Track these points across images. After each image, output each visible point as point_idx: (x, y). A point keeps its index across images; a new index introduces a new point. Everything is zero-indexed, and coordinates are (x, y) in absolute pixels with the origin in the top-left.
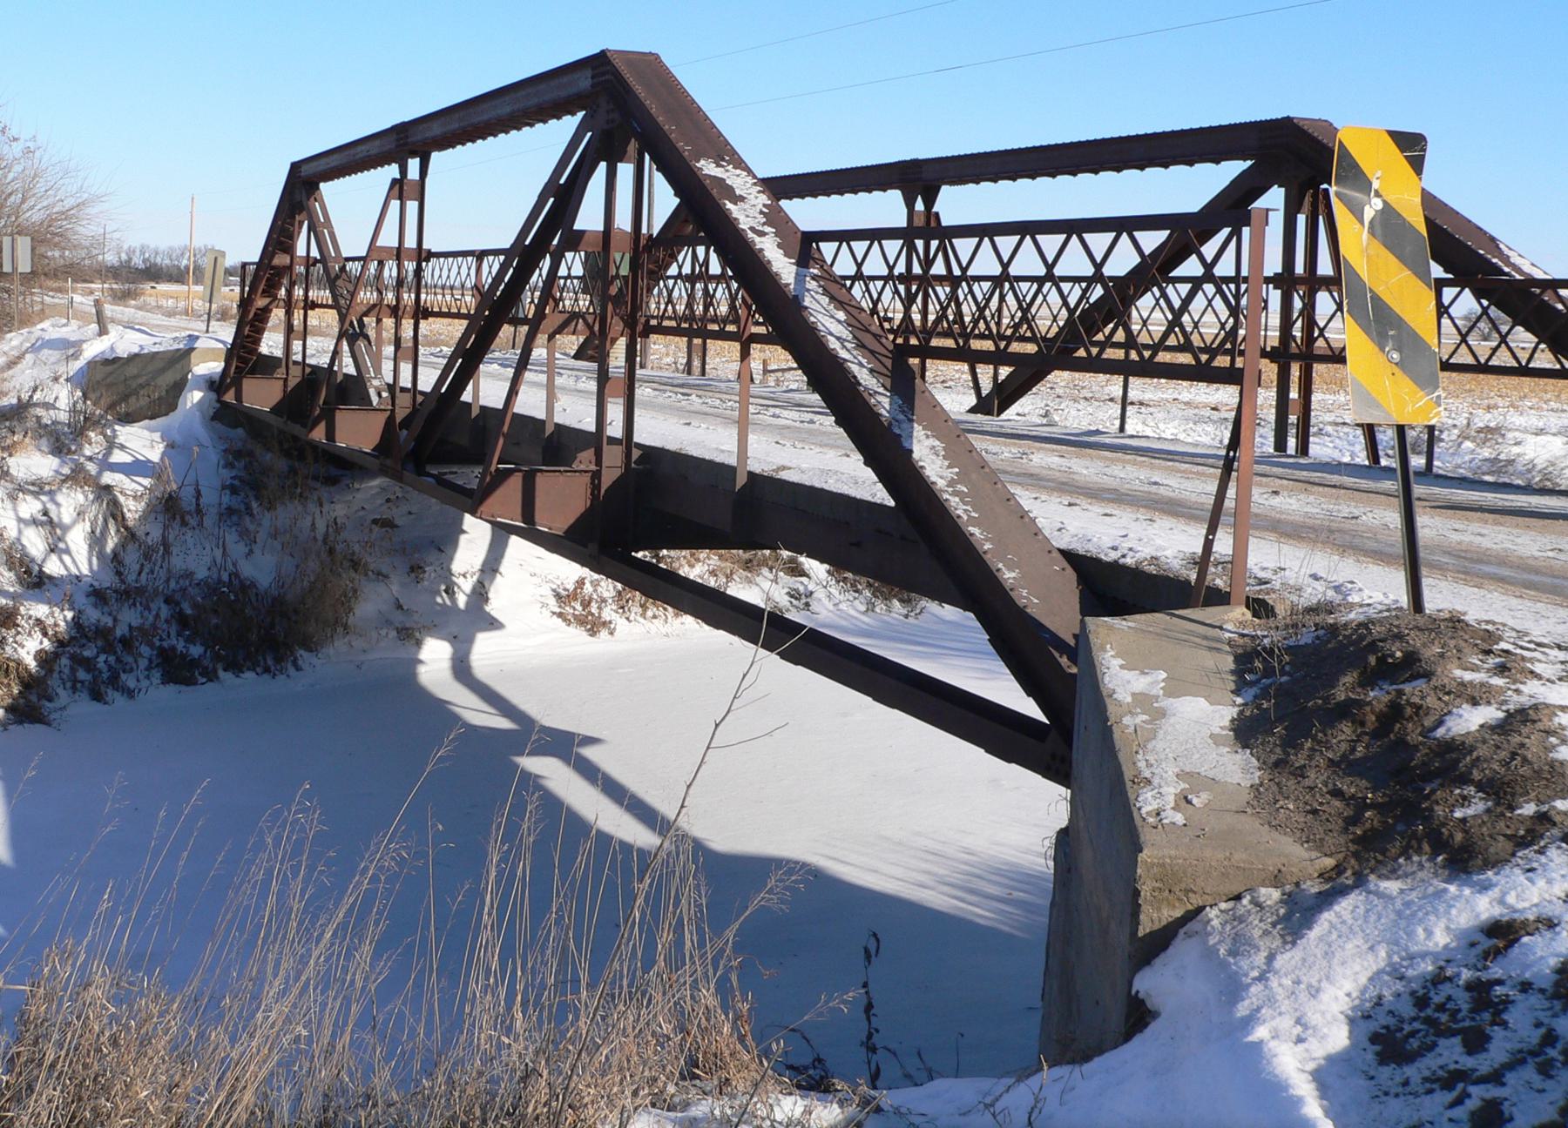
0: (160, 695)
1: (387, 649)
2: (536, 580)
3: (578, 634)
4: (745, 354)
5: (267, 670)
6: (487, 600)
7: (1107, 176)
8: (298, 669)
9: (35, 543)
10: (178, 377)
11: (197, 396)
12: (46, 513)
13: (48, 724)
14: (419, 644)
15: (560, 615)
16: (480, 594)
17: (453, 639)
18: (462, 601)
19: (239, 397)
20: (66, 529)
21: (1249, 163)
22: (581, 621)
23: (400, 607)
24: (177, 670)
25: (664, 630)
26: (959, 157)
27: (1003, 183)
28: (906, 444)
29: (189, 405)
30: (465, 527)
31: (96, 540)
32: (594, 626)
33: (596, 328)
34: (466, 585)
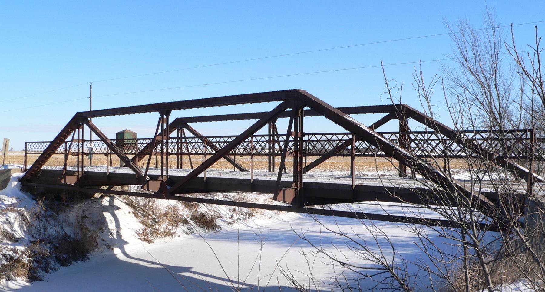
0: (62, 269)
1: (106, 252)
2: (130, 230)
3: (146, 244)
4: (252, 158)
5: (82, 260)
6: (121, 236)
7: (127, 115)
8: (89, 259)
9: (7, 227)
10: (5, 178)
11: (16, 183)
12: (7, 220)
13: (42, 280)
14: (113, 249)
15: (140, 239)
16: (118, 234)
17: (120, 247)
18: (115, 236)
19: (65, 181)
20: (13, 224)
21: (280, 102)
22: (145, 240)
23: (103, 240)
24: (63, 263)
25: (164, 241)
26: (131, 107)
27: (112, 116)
28: (28, 193)
29: (13, 186)
30: (106, 216)
31: (21, 227)
32: (149, 241)
33: (283, 147)
34: (114, 232)
